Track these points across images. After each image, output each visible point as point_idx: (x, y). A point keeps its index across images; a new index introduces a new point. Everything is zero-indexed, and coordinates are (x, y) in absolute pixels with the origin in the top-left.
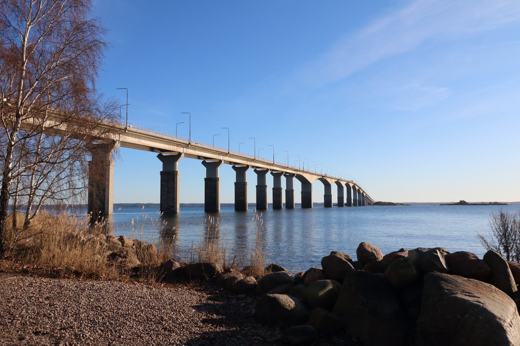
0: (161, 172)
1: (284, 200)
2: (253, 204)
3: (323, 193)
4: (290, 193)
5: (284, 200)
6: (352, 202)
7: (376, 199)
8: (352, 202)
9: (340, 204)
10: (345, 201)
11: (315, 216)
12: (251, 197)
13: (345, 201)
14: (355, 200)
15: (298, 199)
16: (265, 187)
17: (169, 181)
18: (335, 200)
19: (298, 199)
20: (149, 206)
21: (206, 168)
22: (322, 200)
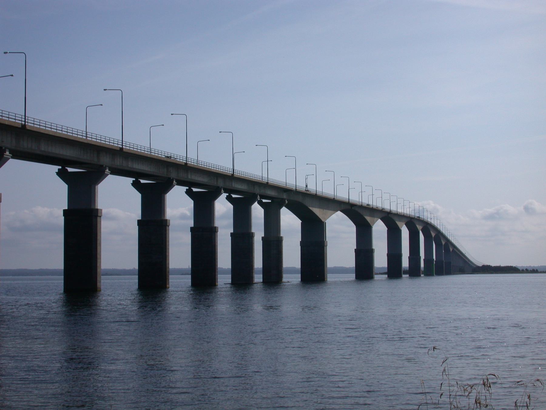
0: (64, 211)
1: (258, 262)
2: (185, 270)
3: (353, 245)
4: (273, 244)
5: (258, 262)
6: (422, 265)
7: (478, 260)
8: (422, 265)
9: (394, 270)
10: (405, 263)
11: (340, 296)
12: (179, 253)
13: (405, 263)
14: (428, 260)
15: (292, 256)
16: (213, 231)
17: (81, 226)
18: (380, 259)
19: (292, 256)
20: (53, 273)
21: (66, 186)
22: (350, 262)
